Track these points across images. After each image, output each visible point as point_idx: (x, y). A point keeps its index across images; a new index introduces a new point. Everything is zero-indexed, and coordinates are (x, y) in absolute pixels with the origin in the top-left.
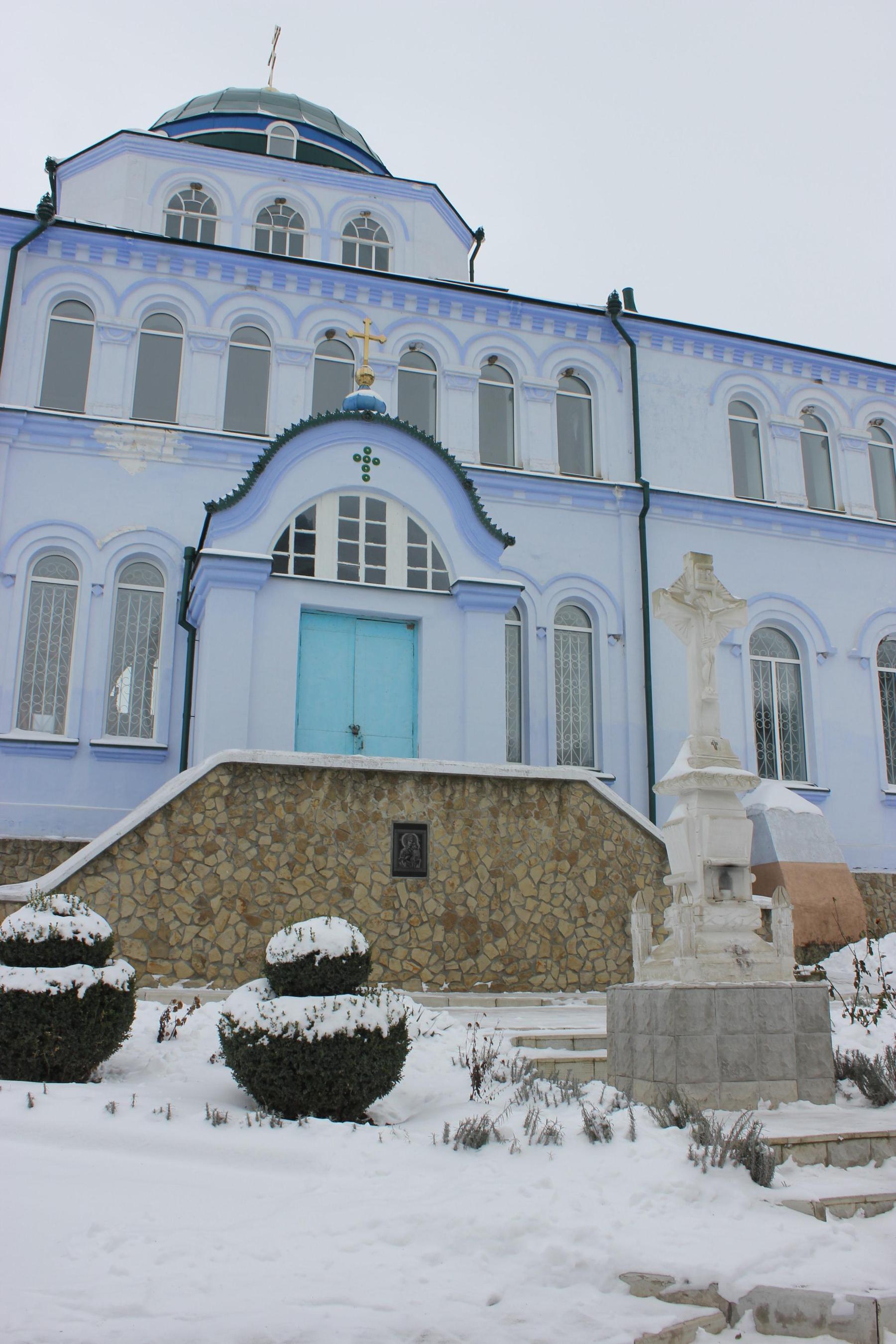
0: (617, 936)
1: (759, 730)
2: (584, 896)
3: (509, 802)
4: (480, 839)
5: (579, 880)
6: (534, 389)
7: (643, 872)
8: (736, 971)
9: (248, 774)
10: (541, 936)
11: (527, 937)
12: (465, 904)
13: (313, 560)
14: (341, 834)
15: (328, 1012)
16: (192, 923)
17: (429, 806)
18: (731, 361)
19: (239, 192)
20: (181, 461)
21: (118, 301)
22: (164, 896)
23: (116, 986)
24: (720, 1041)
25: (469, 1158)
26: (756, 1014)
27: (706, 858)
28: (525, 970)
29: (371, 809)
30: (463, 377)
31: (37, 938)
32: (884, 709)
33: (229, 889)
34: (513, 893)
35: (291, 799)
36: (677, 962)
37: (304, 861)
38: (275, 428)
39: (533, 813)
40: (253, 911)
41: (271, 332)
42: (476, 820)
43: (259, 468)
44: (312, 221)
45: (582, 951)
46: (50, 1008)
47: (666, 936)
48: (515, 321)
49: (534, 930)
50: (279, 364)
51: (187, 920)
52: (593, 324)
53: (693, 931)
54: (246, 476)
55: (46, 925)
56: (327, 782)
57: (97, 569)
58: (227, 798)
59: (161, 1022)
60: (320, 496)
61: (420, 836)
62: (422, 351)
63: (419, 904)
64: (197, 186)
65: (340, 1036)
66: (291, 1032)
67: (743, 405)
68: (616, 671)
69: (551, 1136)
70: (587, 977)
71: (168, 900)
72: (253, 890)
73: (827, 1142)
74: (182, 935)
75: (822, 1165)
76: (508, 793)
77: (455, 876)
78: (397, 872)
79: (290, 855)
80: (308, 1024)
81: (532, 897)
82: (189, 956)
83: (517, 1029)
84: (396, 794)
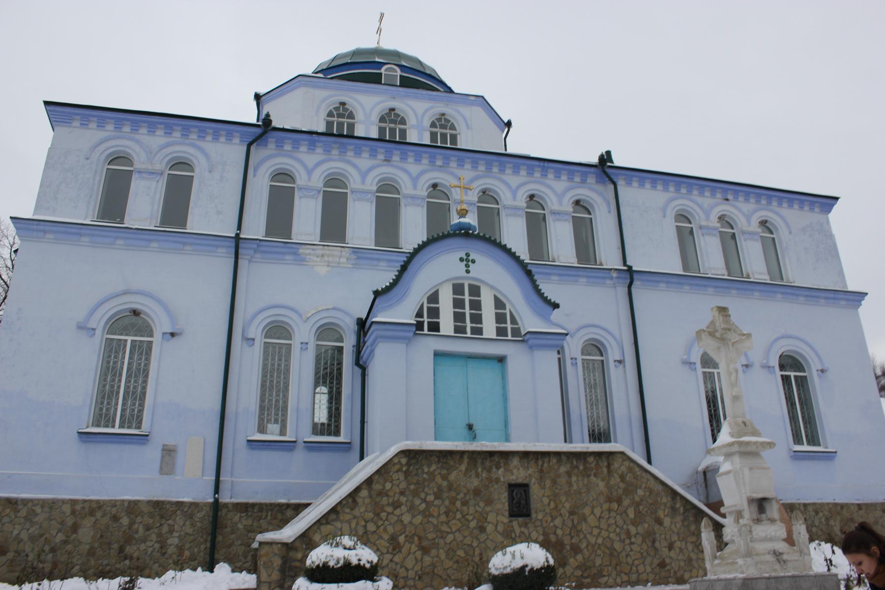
1: (710, 416)
7: (662, 507)
8: (777, 566)
12: (555, 533)
14: (477, 492)
16: (388, 552)
19: (368, 107)
20: (350, 266)
21: (310, 172)
29: (494, 476)
30: (516, 208)
34: (584, 526)
35: (444, 472)
40: (425, 543)
41: (400, 187)
43: (404, 268)
44: (412, 120)
45: (630, 560)
47: (726, 544)
49: (599, 548)
51: (385, 551)
56: (466, 460)
57: (304, 334)
58: (406, 472)
60: (441, 284)
61: (525, 491)
64: (343, 104)
67: (683, 217)
68: (620, 383)
70: (634, 577)
72: (425, 530)
78: (513, 514)
79: (446, 507)
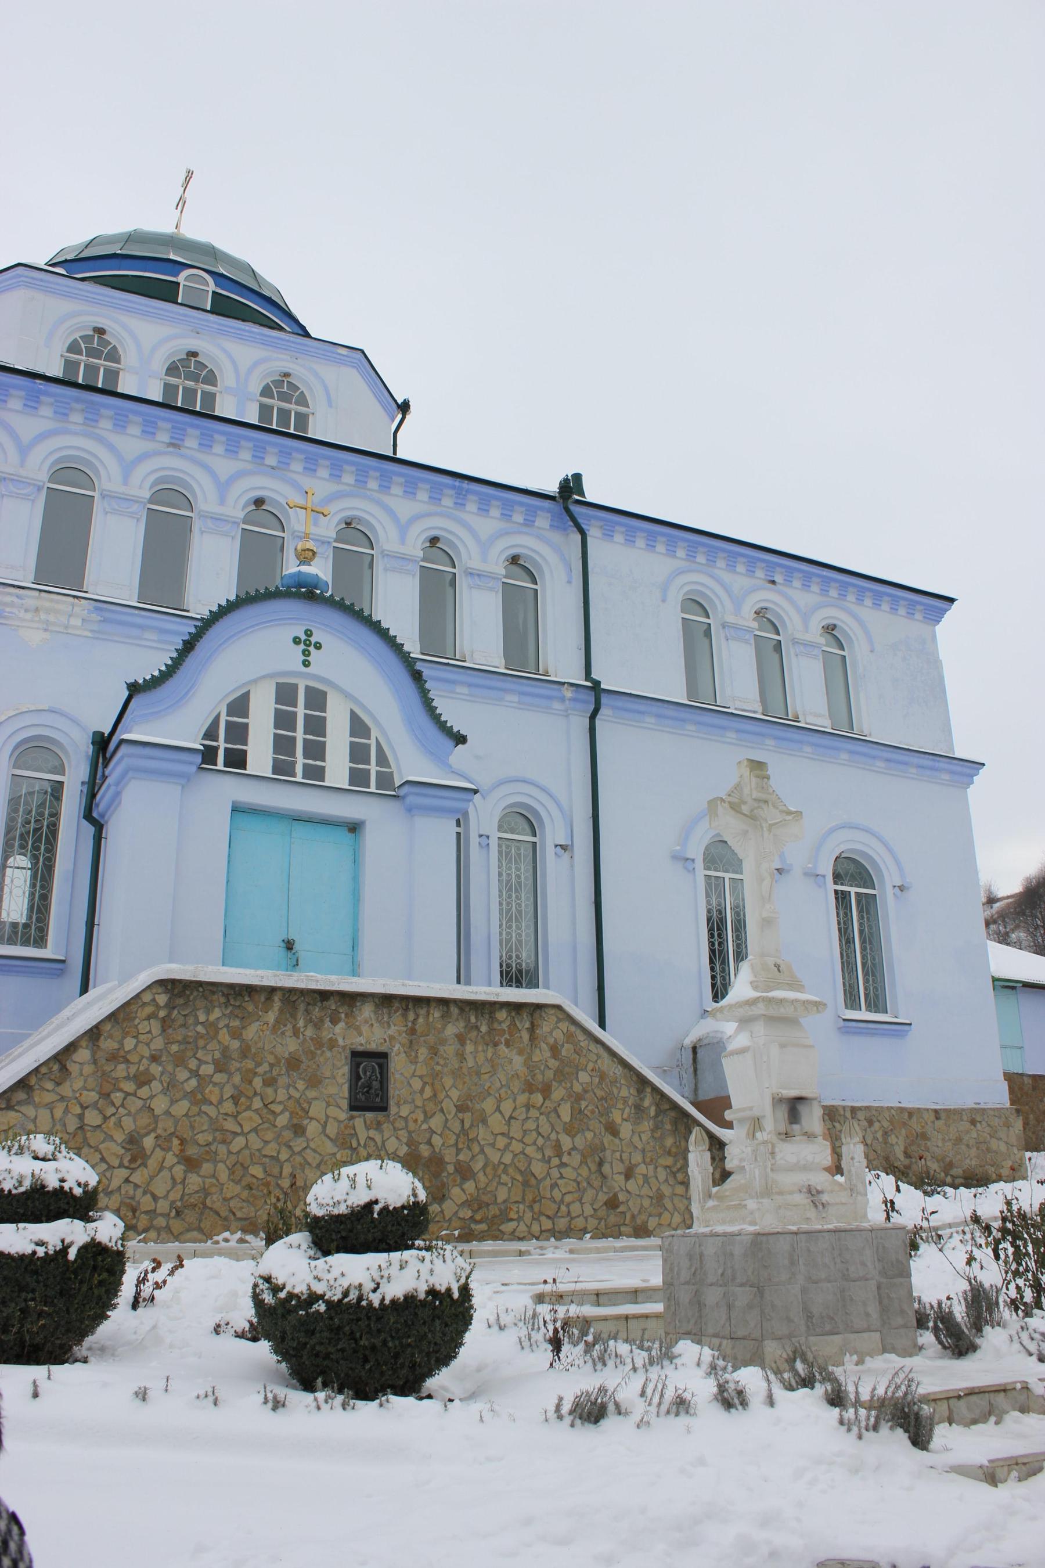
0: (593, 1177)
1: (712, 951)
2: (557, 1133)
3: (477, 1028)
4: (446, 1069)
5: (553, 1115)
6: (479, 575)
7: (620, 1106)
8: (812, 1213)
9: (188, 992)
10: (513, 1179)
11: (497, 1179)
12: (429, 1143)
13: (245, 752)
14: (293, 1063)
15: (394, 1270)
16: (121, 1165)
17: (390, 1032)
18: (684, 556)
19: (147, 342)
20: (90, 634)
22: (89, 1134)
23: (110, 1245)
24: (804, 1291)
25: (587, 1436)
26: (838, 1260)
27: (775, 1090)
28: (494, 1216)
30: (403, 558)
31: (16, 1188)
32: (840, 930)
33: (165, 1126)
35: (236, 1023)
36: (751, 1204)
37: (251, 1094)
38: (201, 601)
39: (503, 1040)
40: (192, 1151)
42: (441, 1048)
43: (189, 646)
46: (36, 1272)
48: (460, 501)
49: (505, 1171)
50: (202, 532)
52: (542, 509)
53: (769, 1170)
54: (175, 655)
55: (27, 1173)
56: (277, 1004)
58: (163, 1020)
59: (137, 1286)
60: (255, 681)
61: (380, 1066)
62: (359, 527)
63: (379, 1144)
64: (100, 331)
65: (410, 1299)
66: (353, 1296)
67: (696, 604)
69: (681, 1405)
70: (562, 1223)
71: (94, 1138)
72: (192, 1127)
73: (948, 1399)
74: (110, 1180)
75: (947, 1424)
76: (476, 1018)
77: (419, 1111)
78: (356, 1106)
79: (235, 1087)
80: (373, 1286)
81: (503, 1134)
82: (117, 1205)
83: (525, 1284)
84: (355, 1018)
